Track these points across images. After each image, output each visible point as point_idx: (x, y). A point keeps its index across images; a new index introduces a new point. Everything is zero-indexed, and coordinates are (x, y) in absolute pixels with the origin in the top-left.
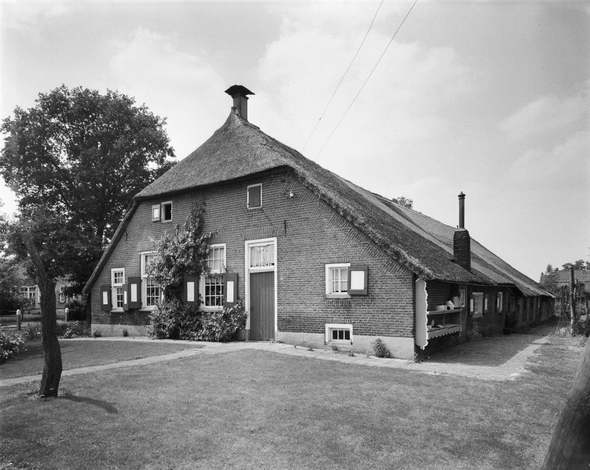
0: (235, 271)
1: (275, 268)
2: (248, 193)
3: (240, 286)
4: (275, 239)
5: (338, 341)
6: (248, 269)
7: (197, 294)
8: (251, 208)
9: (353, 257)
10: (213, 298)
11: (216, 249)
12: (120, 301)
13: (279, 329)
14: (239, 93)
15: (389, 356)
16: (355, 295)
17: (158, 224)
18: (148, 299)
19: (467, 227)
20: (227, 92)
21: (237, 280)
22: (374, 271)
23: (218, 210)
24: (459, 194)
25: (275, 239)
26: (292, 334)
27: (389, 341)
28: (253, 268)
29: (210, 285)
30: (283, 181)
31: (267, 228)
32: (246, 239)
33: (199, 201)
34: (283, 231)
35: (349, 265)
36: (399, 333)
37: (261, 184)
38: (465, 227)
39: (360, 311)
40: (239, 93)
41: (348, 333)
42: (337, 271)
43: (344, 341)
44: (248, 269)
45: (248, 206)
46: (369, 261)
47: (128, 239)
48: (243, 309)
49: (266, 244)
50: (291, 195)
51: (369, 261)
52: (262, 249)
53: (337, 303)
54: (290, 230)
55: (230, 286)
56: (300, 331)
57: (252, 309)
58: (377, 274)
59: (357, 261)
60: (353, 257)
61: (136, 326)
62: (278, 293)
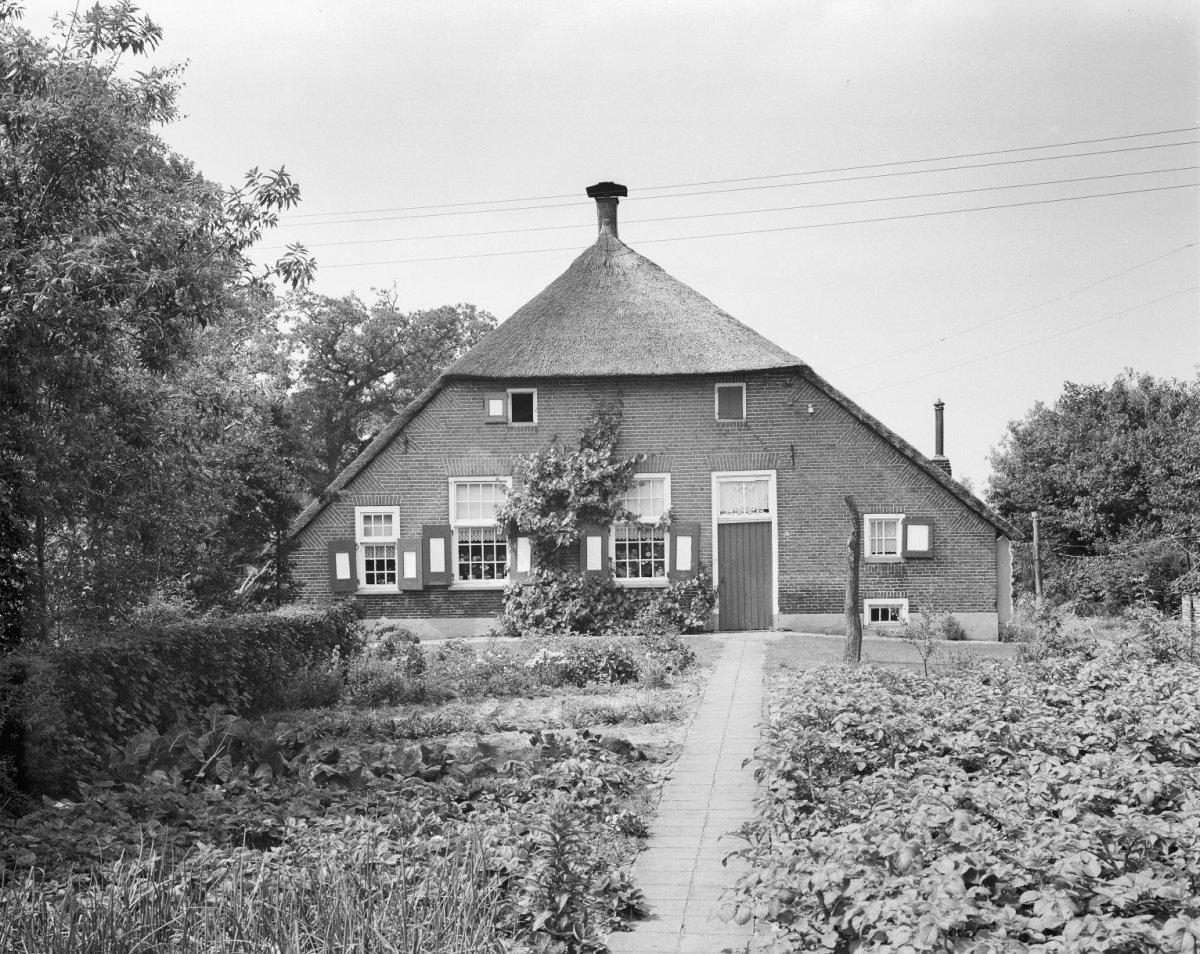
0: (692, 520)
1: (773, 516)
2: (717, 395)
3: (702, 544)
4: (773, 473)
5: (880, 623)
6: (716, 518)
7: (605, 558)
8: (722, 421)
9: (910, 506)
10: (634, 565)
11: (642, 484)
12: (375, 572)
13: (782, 610)
14: (607, 194)
15: (963, 637)
16: (911, 557)
17: (500, 429)
18: (462, 567)
19: (948, 454)
20: (593, 191)
21: (697, 533)
22: (942, 525)
23: (643, 418)
24: (937, 402)
25: (773, 473)
26: (806, 617)
27: (964, 619)
28: (723, 516)
29: (495, 544)
30: (790, 385)
31: (758, 455)
32: (714, 470)
33: (609, 399)
34: (787, 462)
35: (903, 516)
36: (976, 607)
37: (744, 385)
38: (945, 453)
39: (928, 582)
40: (607, 194)
41: (896, 611)
42: (880, 523)
43: (890, 622)
44: (716, 518)
45: (717, 417)
46: (933, 512)
47: (410, 450)
48: (710, 581)
49: (755, 479)
50: (811, 410)
51: (933, 512)
52: (744, 486)
53: (884, 569)
54: (800, 462)
55: (684, 544)
56: (821, 611)
57: (722, 581)
58: (947, 530)
59: (915, 512)
60: (910, 506)
61: (434, 620)
62: (781, 556)
